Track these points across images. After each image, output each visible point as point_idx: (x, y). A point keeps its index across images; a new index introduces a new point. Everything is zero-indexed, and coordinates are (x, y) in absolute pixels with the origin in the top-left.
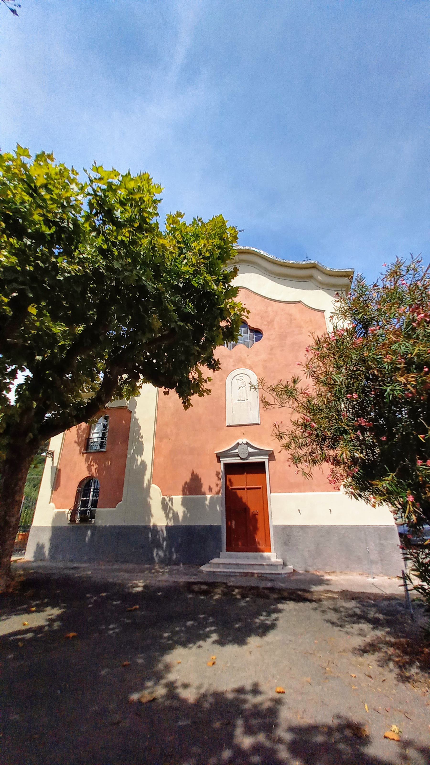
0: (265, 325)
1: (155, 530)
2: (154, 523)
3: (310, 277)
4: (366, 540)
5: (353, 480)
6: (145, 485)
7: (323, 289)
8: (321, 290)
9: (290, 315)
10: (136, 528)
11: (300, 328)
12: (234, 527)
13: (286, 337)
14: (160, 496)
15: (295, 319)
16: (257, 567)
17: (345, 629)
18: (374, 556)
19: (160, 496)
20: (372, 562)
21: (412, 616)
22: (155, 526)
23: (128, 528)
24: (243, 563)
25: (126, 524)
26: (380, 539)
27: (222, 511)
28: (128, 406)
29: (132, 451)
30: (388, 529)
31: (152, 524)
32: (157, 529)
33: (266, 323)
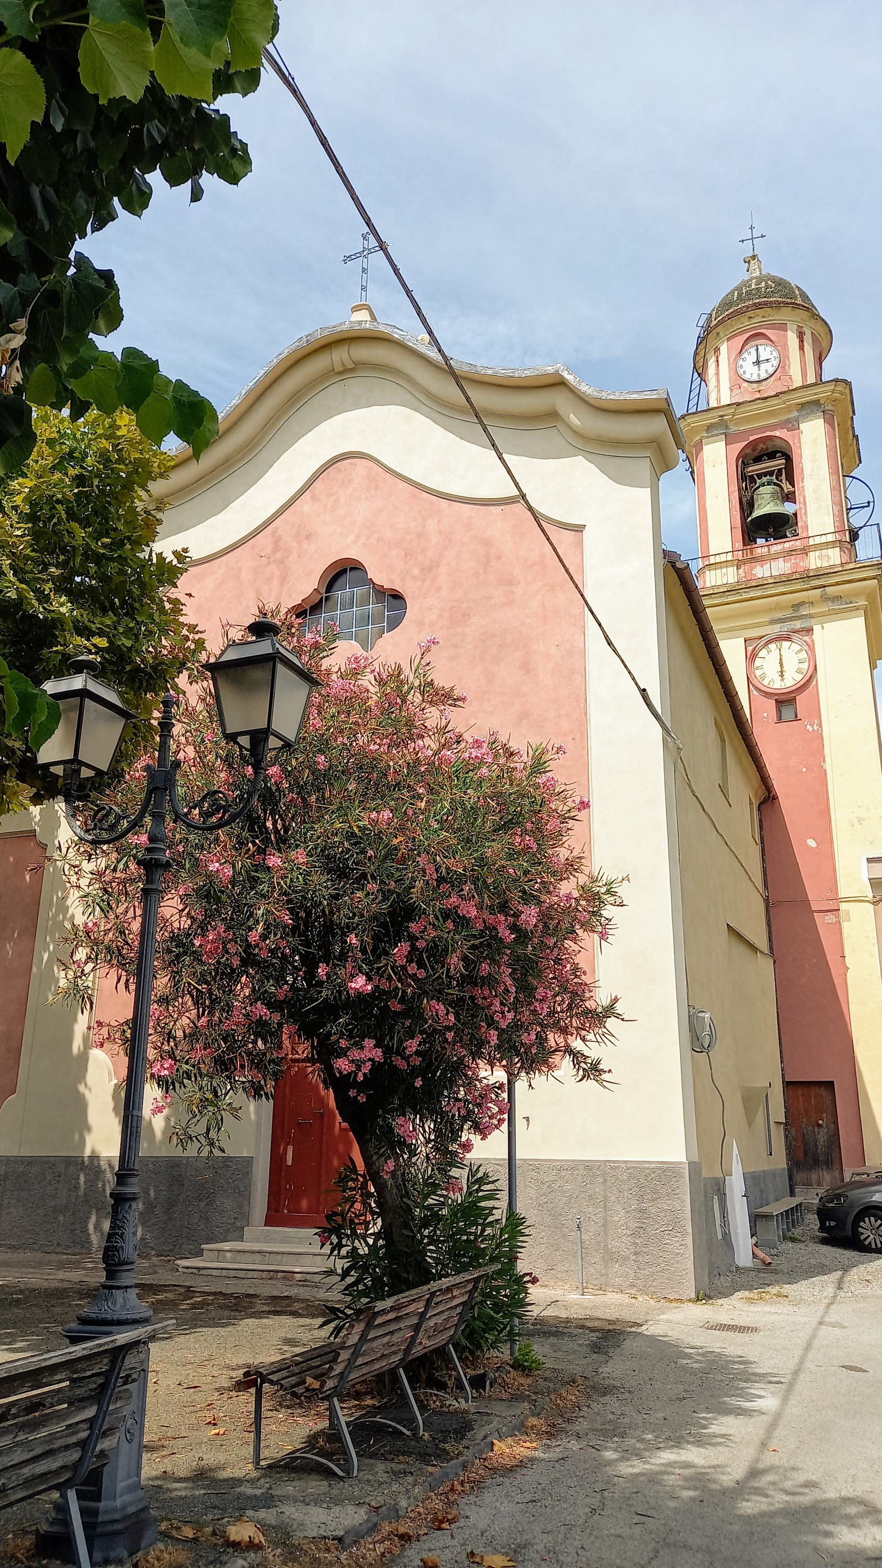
0: (415, 578)
1: (92, 1166)
2: (93, 1151)
3: (552, 416)
4: (606, 1200)
5: (290, 991)
6: (75, 1050)
7: (582, 451)
8: (580, 461)
9: (487, 543)
10: (48, 1163)
11: (511, 584)
12: (289, 1163)
13: (466, 615)
14: (110, 1080)
15: (499, 558)
16: (285, 1258)
17: (242, 1371)
18: (620, 1244)
19: (110, 1080)
20: (610, 1257)
21: (517, 1365)
22: (94, 1157)
23: (30, 1161)
24: (275, 1250)
25: (24, 1153)
26: (641, 1199)
27: (259, 1123)
28: (38, 830)
29: (46, 956)
30: (666, 1171)
31: (87, 1152)
32: (99, 1166)
33: (416, 572)
